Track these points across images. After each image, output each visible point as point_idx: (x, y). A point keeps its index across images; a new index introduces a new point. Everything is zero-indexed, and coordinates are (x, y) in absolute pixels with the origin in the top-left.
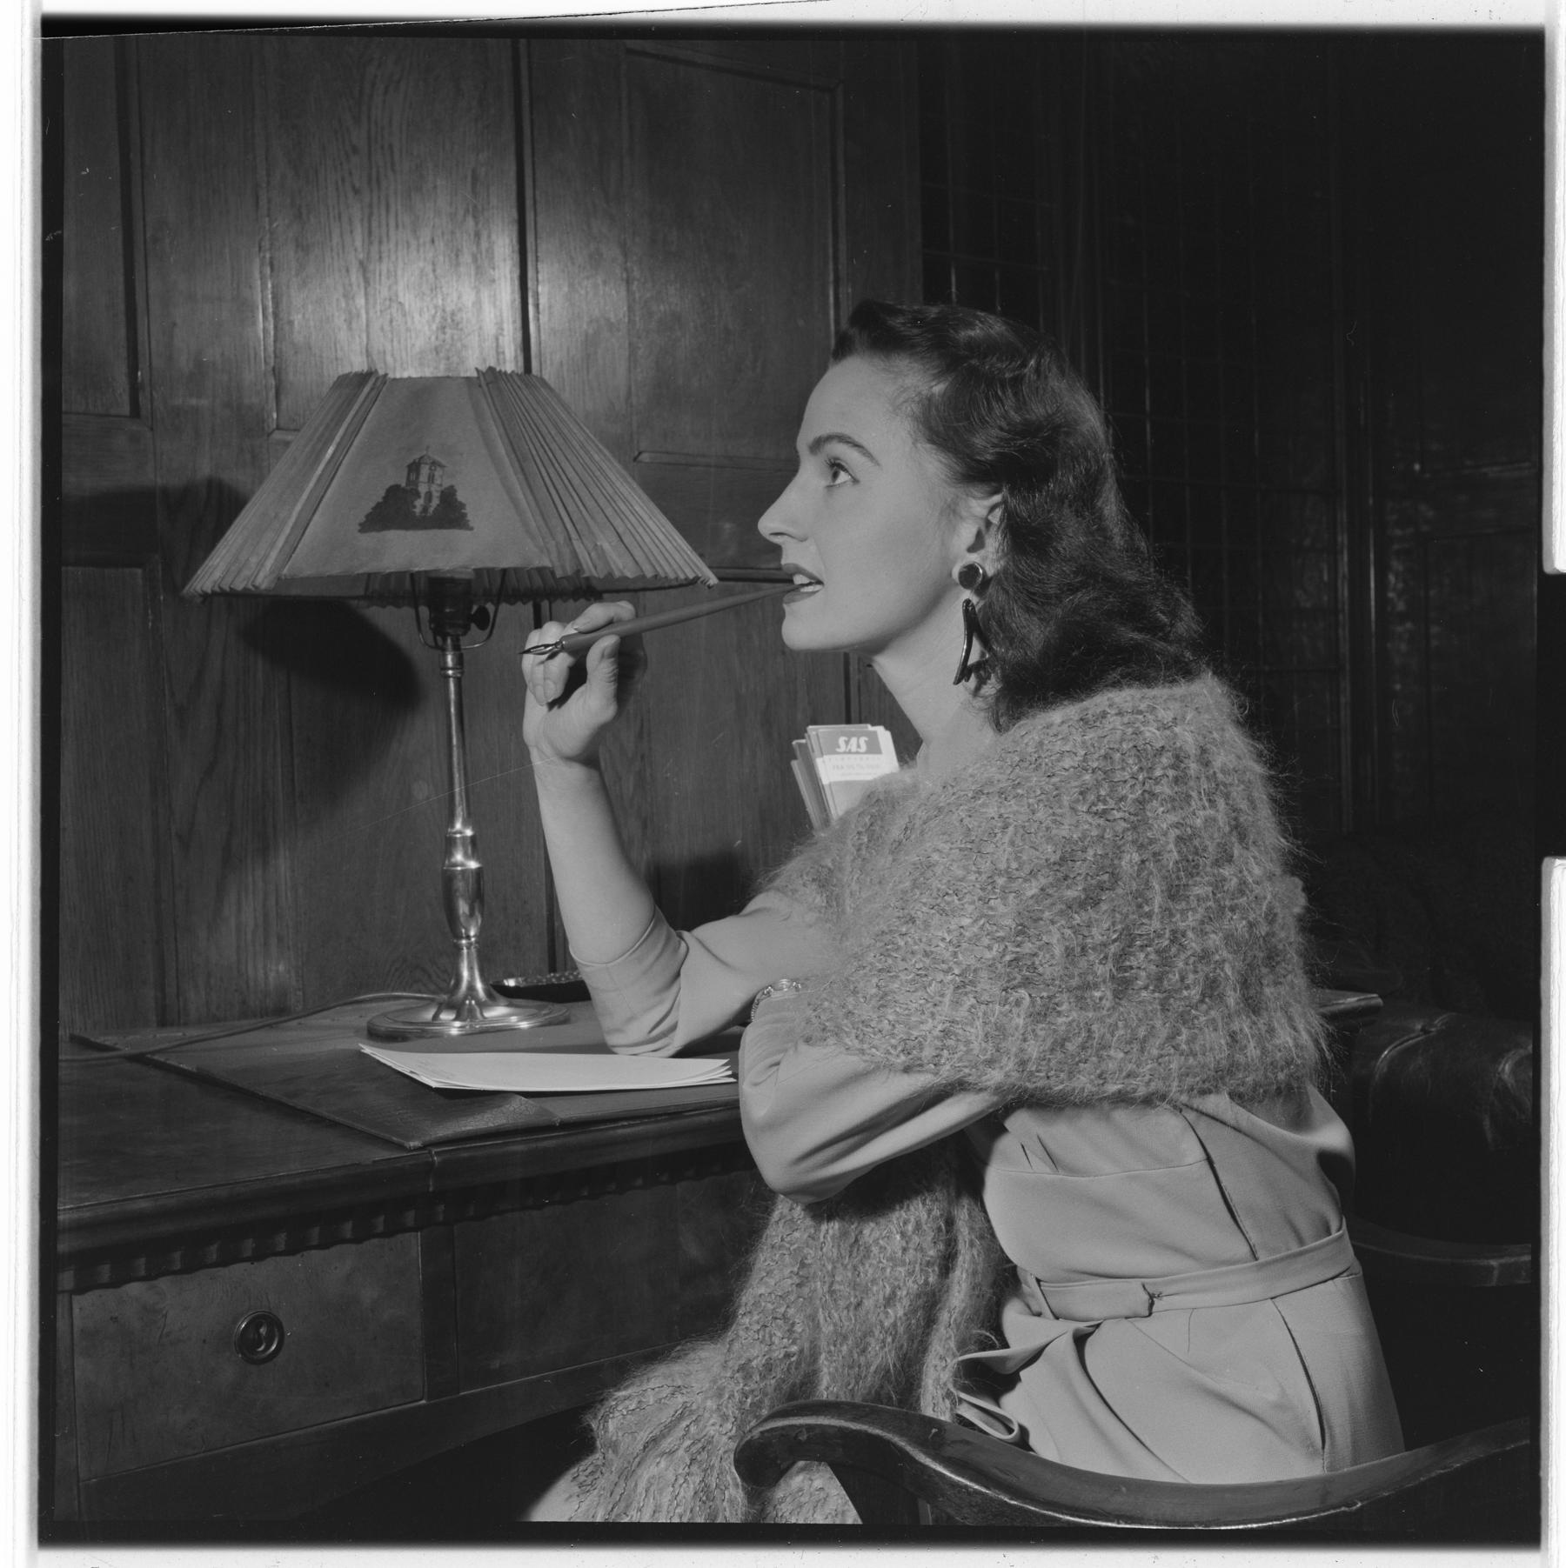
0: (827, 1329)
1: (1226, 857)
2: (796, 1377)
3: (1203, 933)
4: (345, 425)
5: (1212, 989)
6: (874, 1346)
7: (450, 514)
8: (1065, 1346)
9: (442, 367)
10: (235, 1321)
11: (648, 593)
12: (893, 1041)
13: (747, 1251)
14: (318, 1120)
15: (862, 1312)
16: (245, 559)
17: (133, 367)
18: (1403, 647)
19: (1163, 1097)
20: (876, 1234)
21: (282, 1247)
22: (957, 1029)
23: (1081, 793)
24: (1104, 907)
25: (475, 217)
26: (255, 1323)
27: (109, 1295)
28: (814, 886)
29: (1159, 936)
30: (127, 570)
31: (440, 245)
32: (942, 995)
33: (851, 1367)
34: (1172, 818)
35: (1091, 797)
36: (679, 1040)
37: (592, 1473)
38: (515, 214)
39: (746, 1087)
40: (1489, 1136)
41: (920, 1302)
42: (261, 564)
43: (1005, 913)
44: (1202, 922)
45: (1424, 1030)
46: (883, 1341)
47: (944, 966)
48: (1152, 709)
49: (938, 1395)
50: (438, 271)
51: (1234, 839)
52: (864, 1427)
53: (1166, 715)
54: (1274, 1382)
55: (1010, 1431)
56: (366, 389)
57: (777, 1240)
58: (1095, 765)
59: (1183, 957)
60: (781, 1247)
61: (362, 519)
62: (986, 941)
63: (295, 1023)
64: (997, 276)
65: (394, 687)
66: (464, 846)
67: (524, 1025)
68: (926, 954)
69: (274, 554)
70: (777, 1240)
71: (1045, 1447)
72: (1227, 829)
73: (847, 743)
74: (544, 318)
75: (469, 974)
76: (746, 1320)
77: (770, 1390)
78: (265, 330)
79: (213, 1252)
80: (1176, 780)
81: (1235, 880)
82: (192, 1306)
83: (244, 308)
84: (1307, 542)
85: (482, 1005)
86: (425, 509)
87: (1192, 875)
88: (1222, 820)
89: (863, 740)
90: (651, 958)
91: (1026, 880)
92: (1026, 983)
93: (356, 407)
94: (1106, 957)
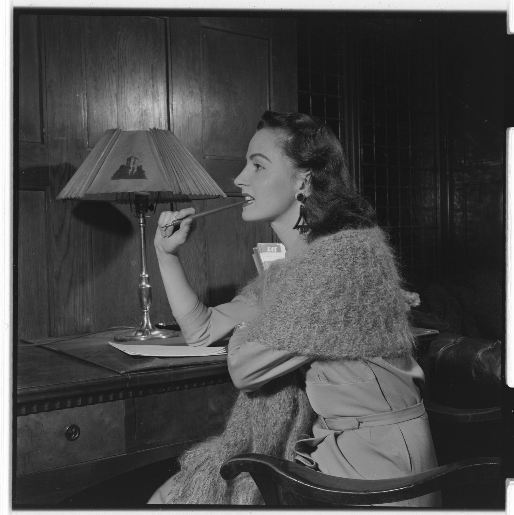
0: (255, 433)
1: (380, 283)
2: (245, 448)
3: (373, 306)
4: (108, 146)
5: (375, 324)
6: (270, 439)
7: (140, 174)
8: (331, 437)
9: (142, 128)
10: (65, 427)
11: (208, 200)
12: (275, 340)
13: (230, 408)
14: (94, 365)
15: (266, 428)
16: (75, 188)
17: (42, 127)
18: (459, 220)
19: (361, 358)
20: (271, 403)
21: (80, 404)
22: (295, 336)
23: (334, 262)
24: (341, 298)
25: (152, 80)
26: (71, 428)
27: (25, 417)
28: (254, 294)
29: (359, 307)
30: (40, 192)
31: (141, 89)
32: (290, 326)
33: (263, 446)
34: (363, 270)
35: (337, 263)
36: (210, 341)
37: (180, 477)
38: (165, 79)
39: (229, 355)
40: (474, 375)
41: (285, 425)
42: (80, 190)
43: (310, 299)
44: (372, 303)
45: (455, 342)
46: (273, 437)
47: (291, 316)
48: (357, 236)
49: (290, 454)
50: (141, 97)
51: (383, 277)
52: (260, 461)
53: (361, 238)
54: (397, 450)
55: (312, 463)
56: (114, 135)
57: (240, 404)
58: (338, 253)
59: (366, 314)
60: (241, 406)
61: (112, 175)
62: (304, 308)
63: (91, 336)
64: (325, 99)
65: (124, 229)
66: (146, 280)
67: (164, 337)
68: (285, 312)
69: (84, 186)
70: (240, 404)
71: (325, 470)
72: (380, 274)
73: (270, 249)
74: (174, 112)
75: (146, 320)
76: (229, 429)
77: (235, 451)
78: (84, 115)
79: (58, 404)
80: (364, 258)
81: (383, 290)
82: (52, 421)
83: (78, 108)
84: (427, 186)
85: (151, 331)
86: (132, 173)
87: (369, 288)
88: (379, 271)
89: (275, 248)
90: (198, 315)
91: (316, 289)
92: (317, 322)
93: (111, 140)
94: (342, 314)
